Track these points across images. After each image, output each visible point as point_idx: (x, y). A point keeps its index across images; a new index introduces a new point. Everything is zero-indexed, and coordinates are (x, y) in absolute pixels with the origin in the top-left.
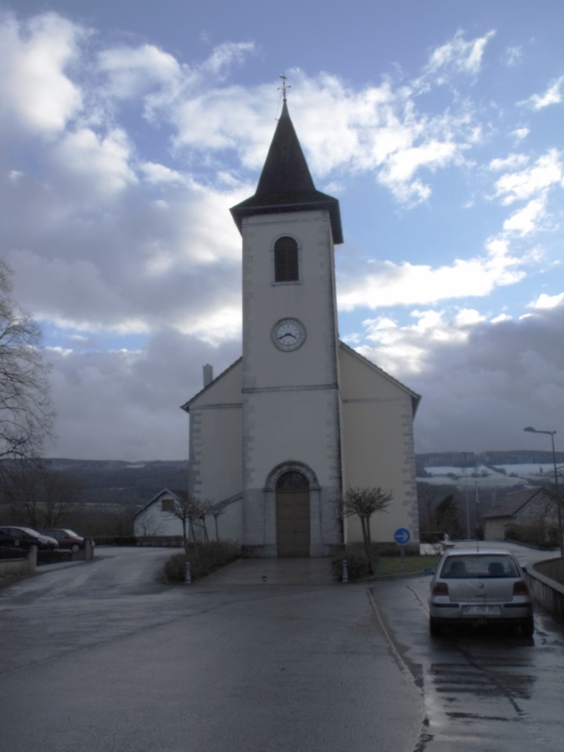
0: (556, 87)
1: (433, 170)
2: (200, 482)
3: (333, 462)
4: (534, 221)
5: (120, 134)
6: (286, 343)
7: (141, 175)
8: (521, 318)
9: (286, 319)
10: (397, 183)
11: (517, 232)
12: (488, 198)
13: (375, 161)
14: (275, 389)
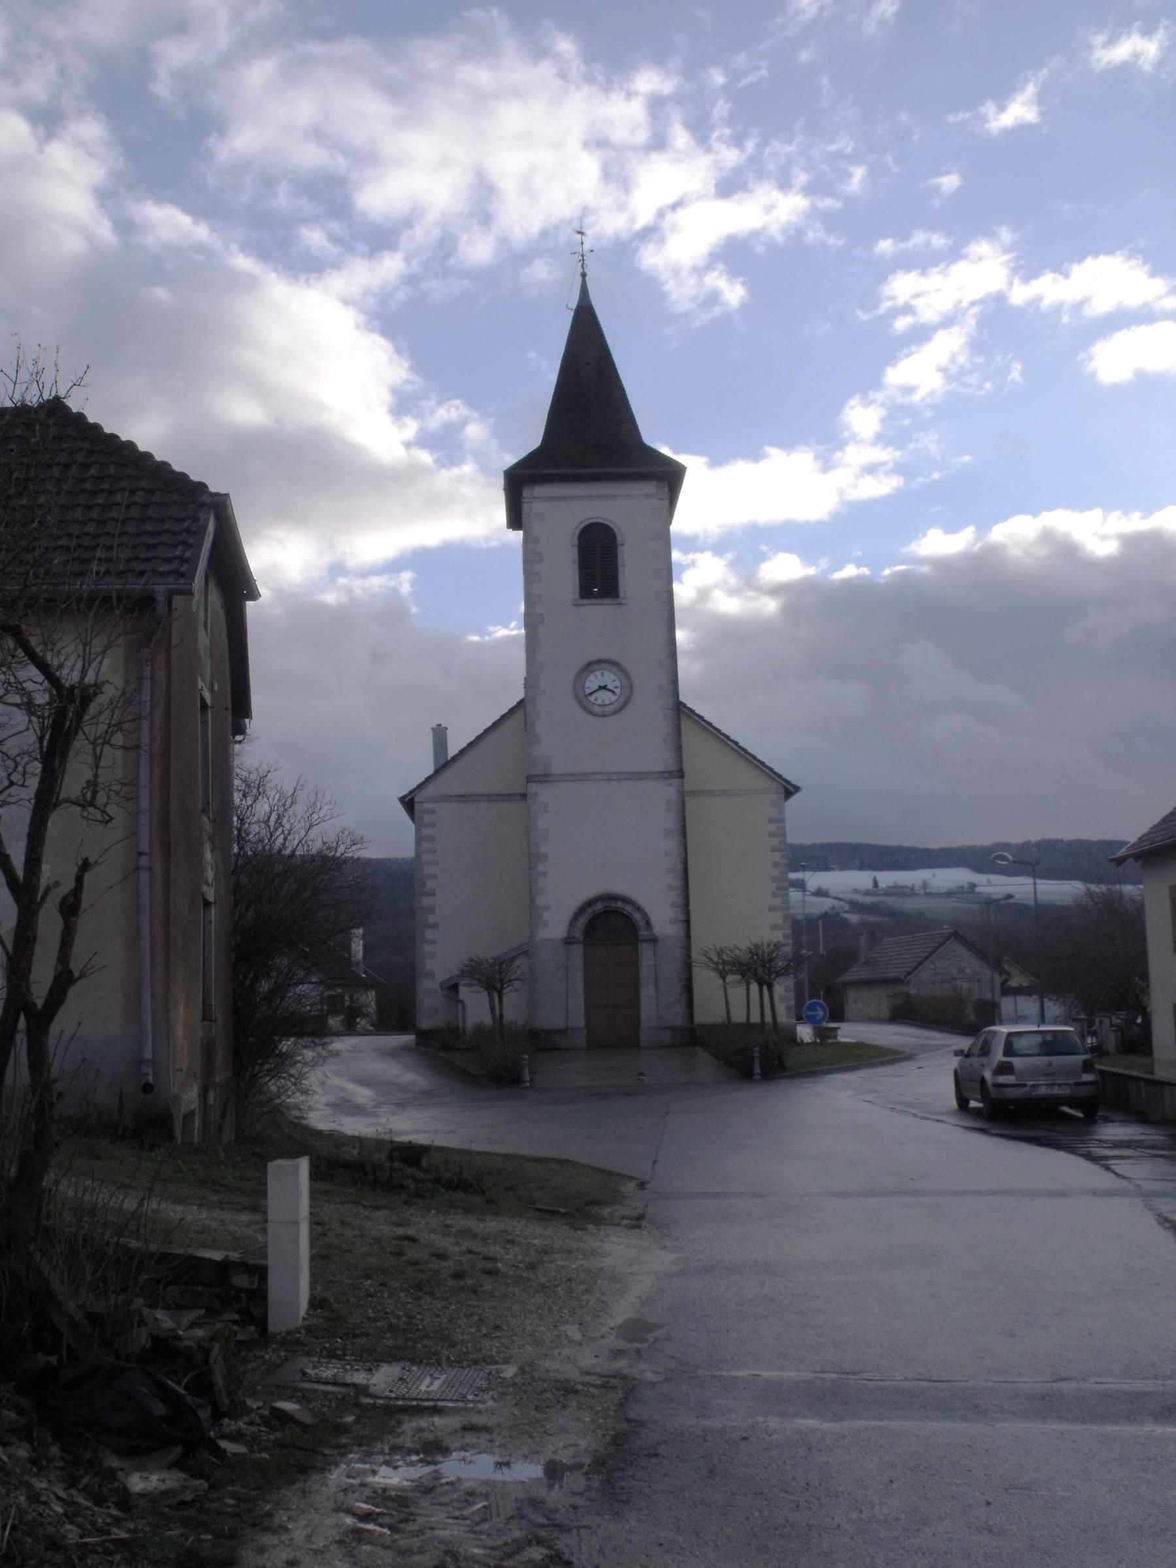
0: (1031, 89)
1: (760, 249)
2: (435, 926)
3: (675, 897)
4: (943, 370)
5: (92, 129)
6: (599, 702)
7: (126, 227)
8: (887, 572)
9: (599, 662)
10: (676, 271)
11: (909, 390)
12: (862, 316)
13: (632, 220)
14: (582, 777)
